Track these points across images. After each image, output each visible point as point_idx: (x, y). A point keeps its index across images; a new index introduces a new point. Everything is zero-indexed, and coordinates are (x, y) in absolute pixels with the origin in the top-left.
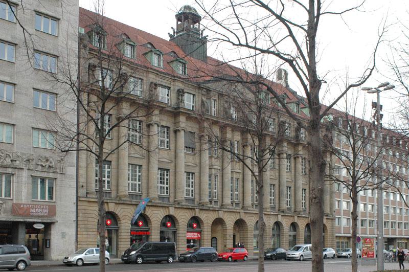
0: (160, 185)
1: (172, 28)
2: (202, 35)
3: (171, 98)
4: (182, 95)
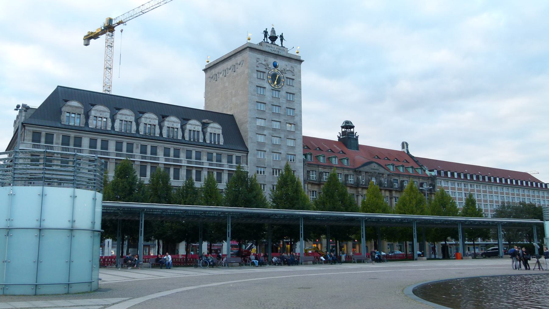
1: (339, 133)
2: (355, 136)
3: (342, 179)
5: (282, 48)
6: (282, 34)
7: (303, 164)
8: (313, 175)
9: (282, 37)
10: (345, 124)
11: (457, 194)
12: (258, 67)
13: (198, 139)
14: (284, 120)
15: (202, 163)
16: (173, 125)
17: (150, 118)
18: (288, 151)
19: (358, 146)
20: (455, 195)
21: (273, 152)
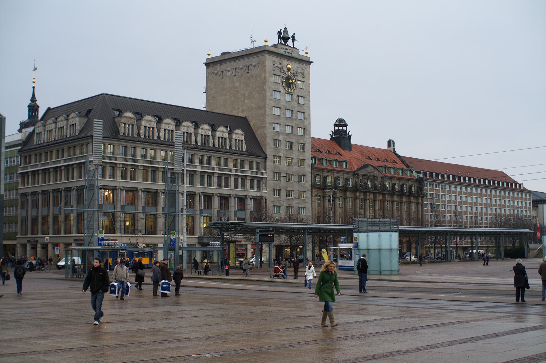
1: (332, 131)
5: (294, 49)
6: (294, 34)
9: (293, 37)
10: (339, 123)
12: (274, 70)
13: (153, 136)
14: (296, 124)
15: (196, 167)
16: (205, 133)
17: (187, 126)
19: (351, 146)
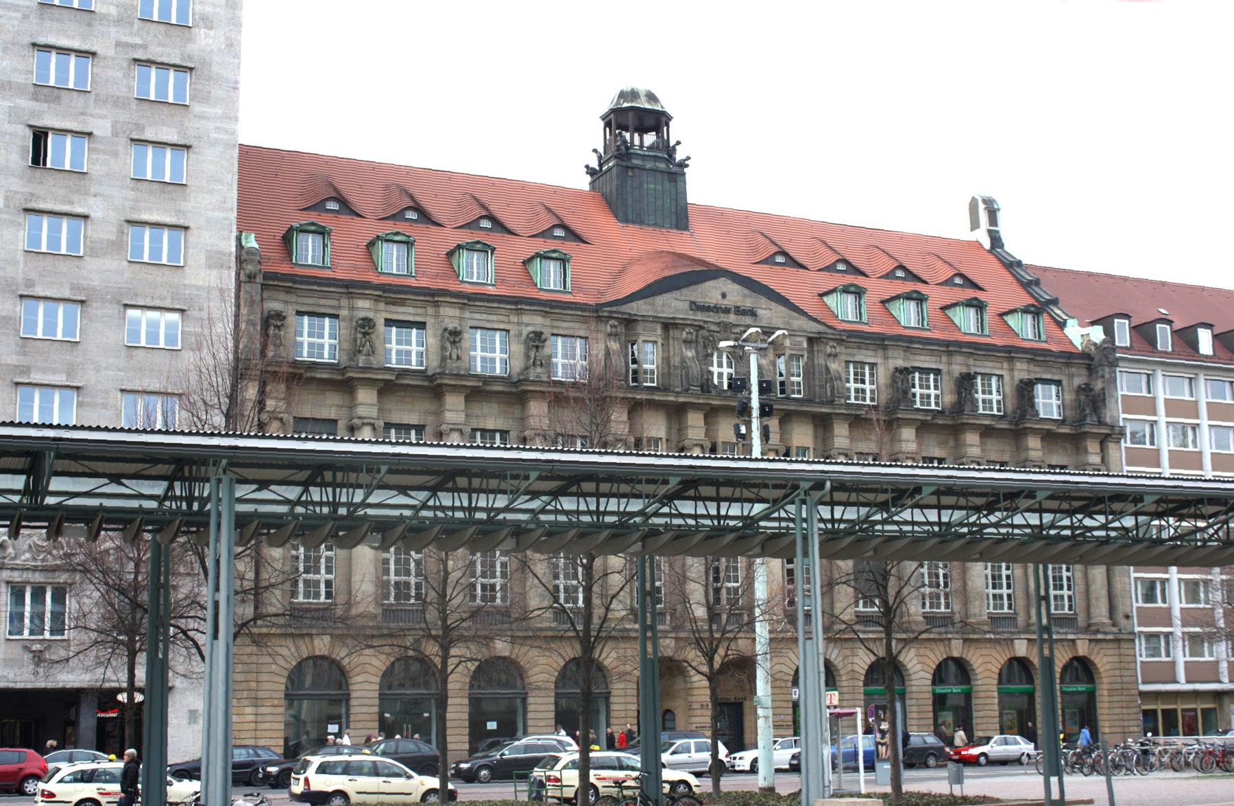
0: (991, 591)
1: (595, 151)
4: (537, 347)
7: (238, 274)
8: (928, 387)
11: (1205, 433)
14: (118, 44)
18: (138, 201)
20: (1194, 441)
21: (27, 210)
